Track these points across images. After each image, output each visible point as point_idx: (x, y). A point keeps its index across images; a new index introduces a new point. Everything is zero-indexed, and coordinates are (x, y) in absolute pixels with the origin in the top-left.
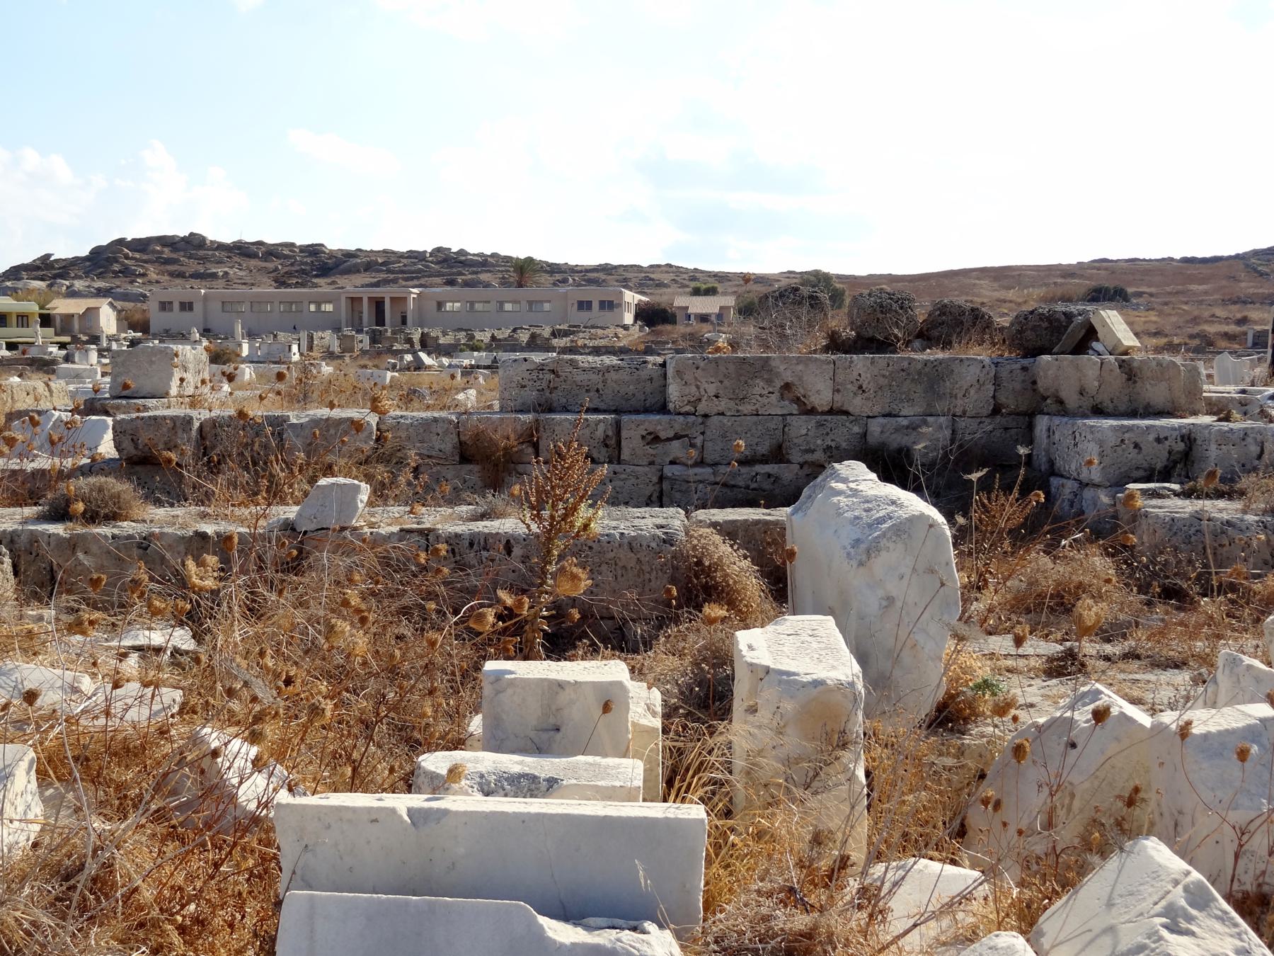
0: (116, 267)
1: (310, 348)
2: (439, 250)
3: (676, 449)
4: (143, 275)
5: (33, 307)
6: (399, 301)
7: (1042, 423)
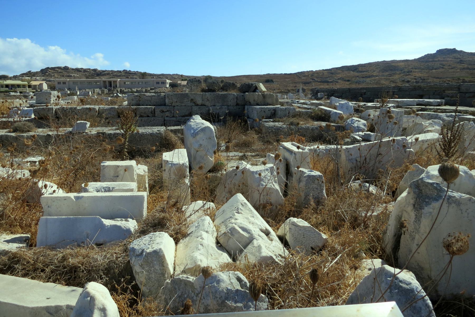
0: (47, 74)
1: (94, 93)
2: (124, 70)
3: (167, 114)
4: (54, 76)
5: (26, 83)
6: (115, 82)
7: (246, 107)
